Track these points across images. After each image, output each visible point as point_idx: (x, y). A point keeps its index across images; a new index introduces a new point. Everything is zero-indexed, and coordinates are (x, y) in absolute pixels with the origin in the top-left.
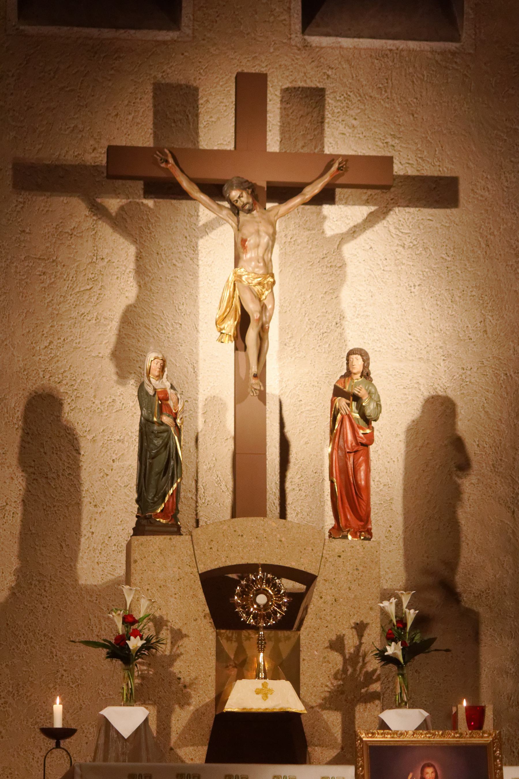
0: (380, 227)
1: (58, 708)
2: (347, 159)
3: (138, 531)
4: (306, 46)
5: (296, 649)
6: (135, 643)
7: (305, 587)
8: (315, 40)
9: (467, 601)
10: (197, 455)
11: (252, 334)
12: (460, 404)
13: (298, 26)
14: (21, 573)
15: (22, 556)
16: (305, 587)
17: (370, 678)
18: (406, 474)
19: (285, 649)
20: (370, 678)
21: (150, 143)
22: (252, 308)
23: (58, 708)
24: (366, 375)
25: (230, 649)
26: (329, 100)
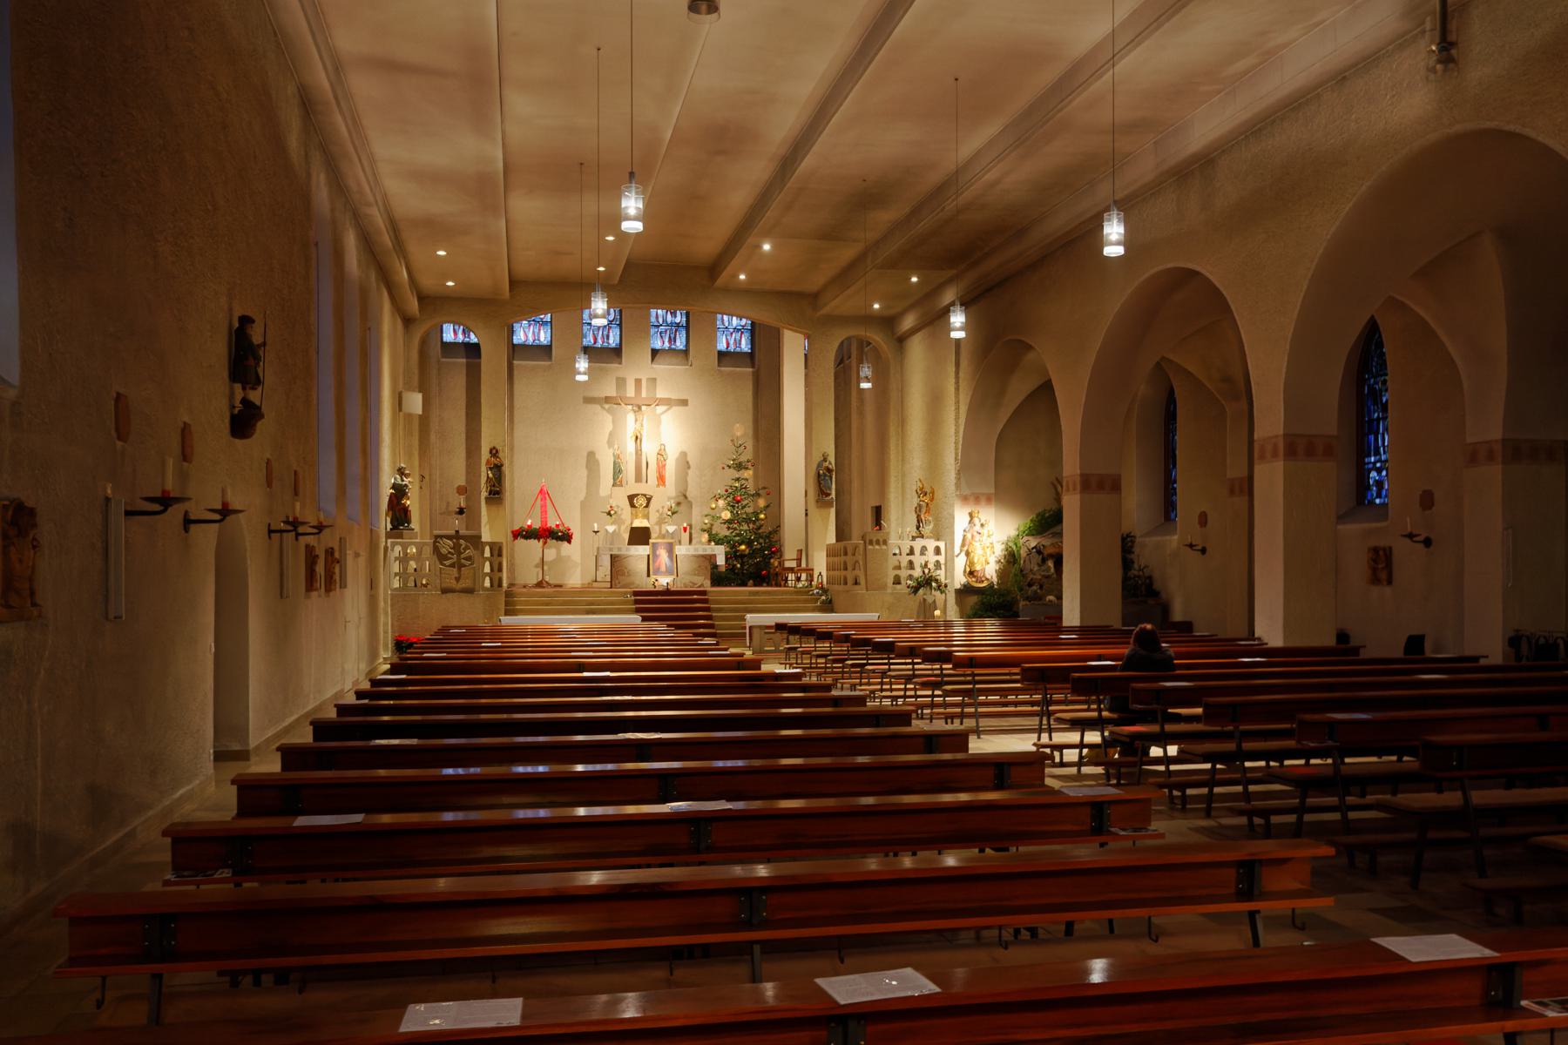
0: (670, 411)
1: (596, 525)
2: (660, 399)
3: (613, 485)
4: (652, 368)
5: (648, 513)
6: (612, 512)
7: (755, 946)
8: (655, 366)
9: (689, 499)
10: (820, 484)
11: (638, 440)
12: (689, 454)
13: (650, 362)
14: (587, 493)
15: (587, 489)
16: (755, 946)
17: (665, 518)
18: (378, 474)
19: (646, 512)
20: (665, 518)
21: (615, 395)
22: (639, 435)
23: (596, 525)
24: (664, 450)
25: (634, 512)
26: (658, 382)
